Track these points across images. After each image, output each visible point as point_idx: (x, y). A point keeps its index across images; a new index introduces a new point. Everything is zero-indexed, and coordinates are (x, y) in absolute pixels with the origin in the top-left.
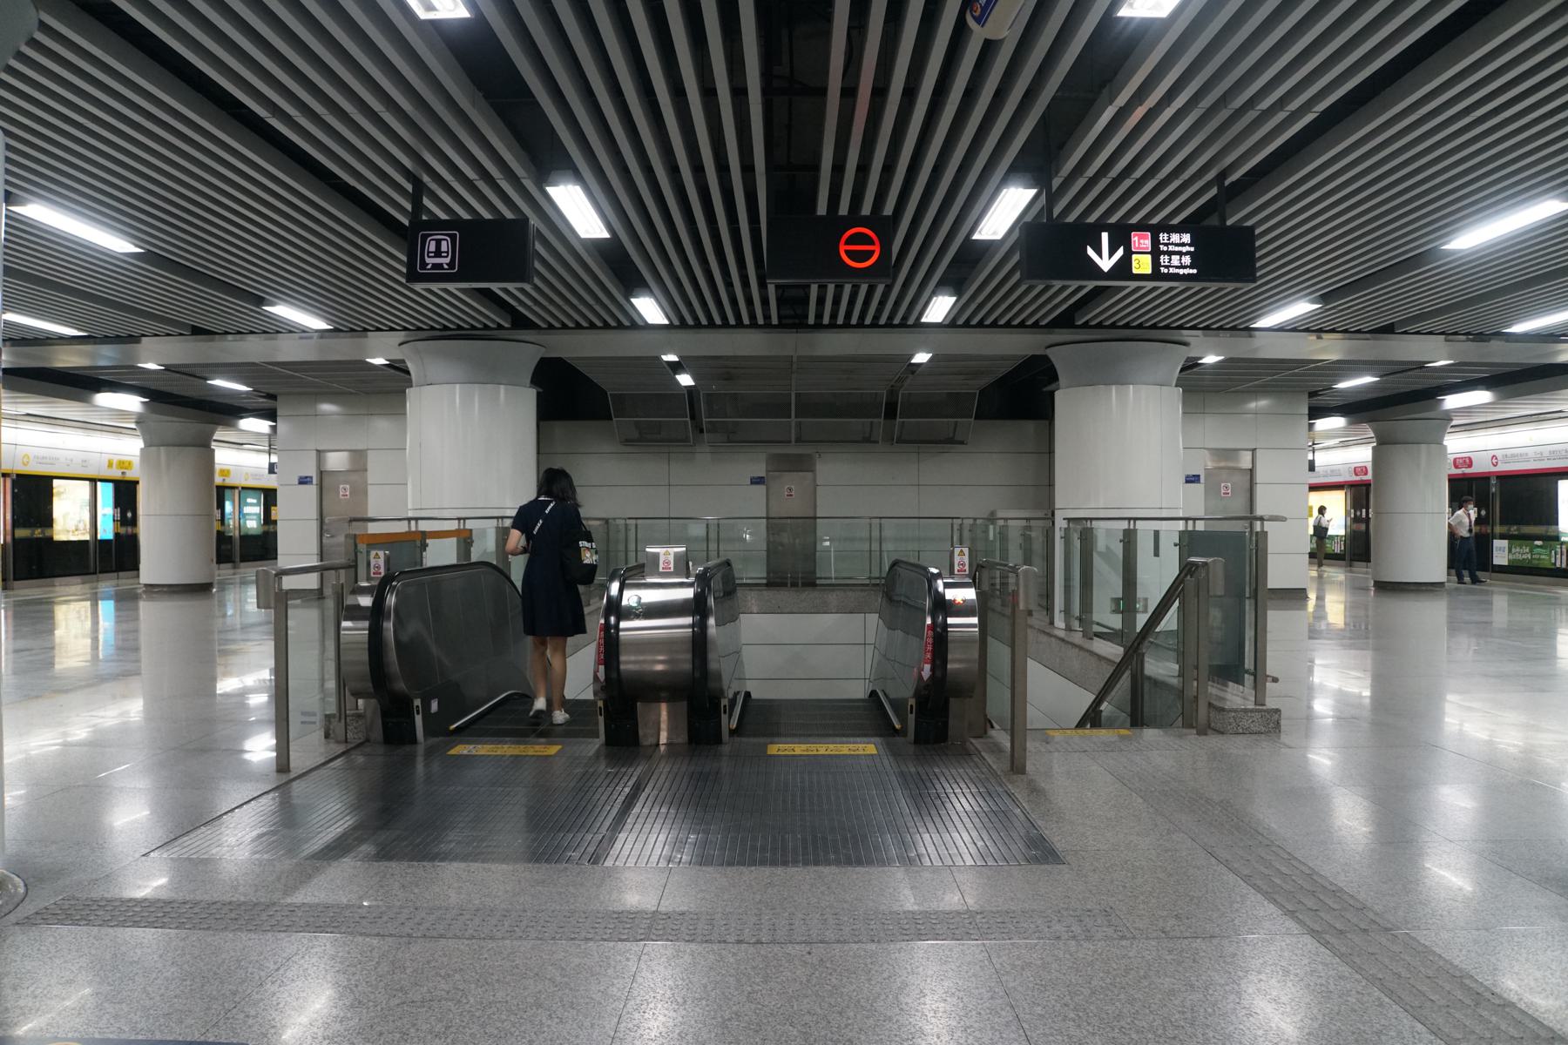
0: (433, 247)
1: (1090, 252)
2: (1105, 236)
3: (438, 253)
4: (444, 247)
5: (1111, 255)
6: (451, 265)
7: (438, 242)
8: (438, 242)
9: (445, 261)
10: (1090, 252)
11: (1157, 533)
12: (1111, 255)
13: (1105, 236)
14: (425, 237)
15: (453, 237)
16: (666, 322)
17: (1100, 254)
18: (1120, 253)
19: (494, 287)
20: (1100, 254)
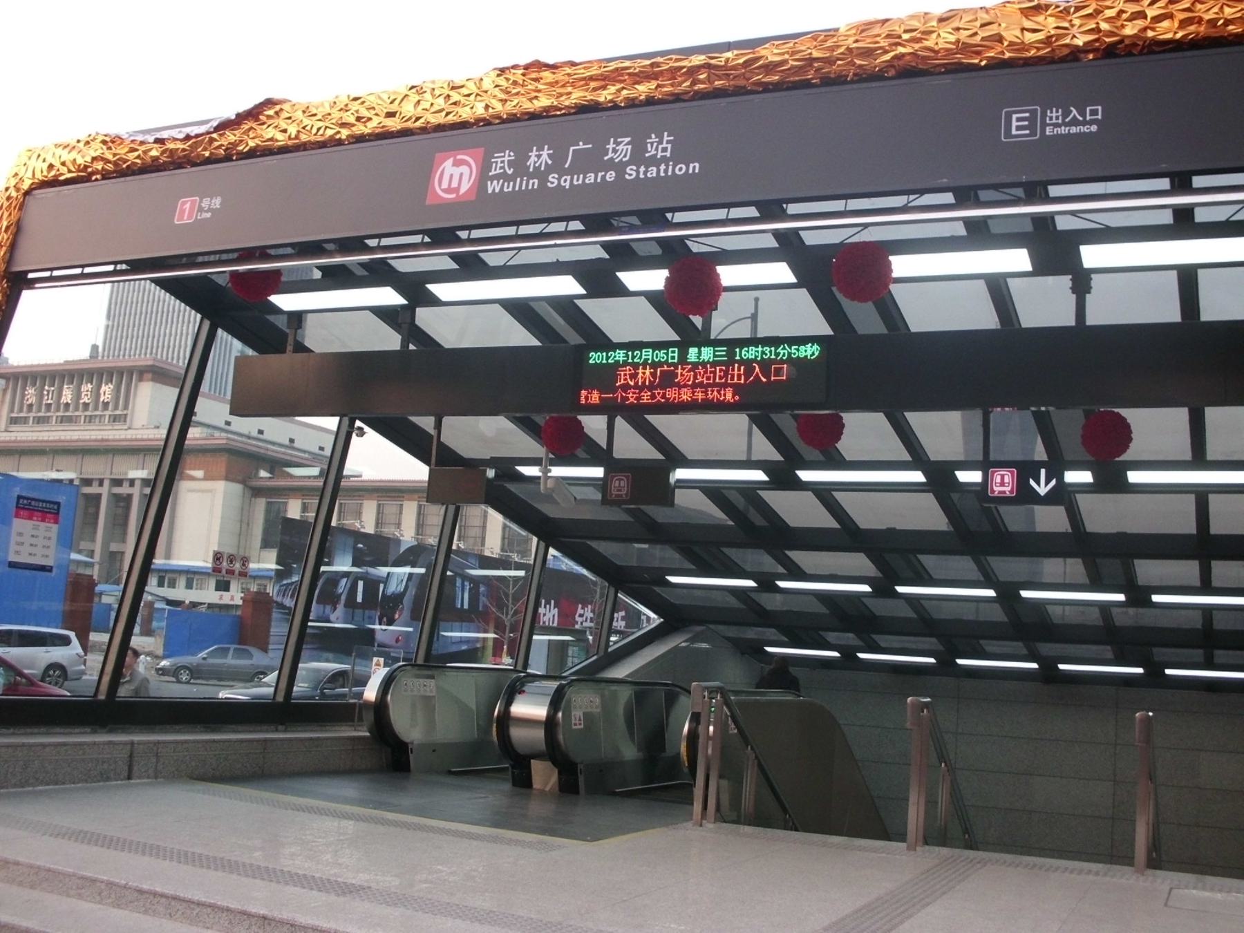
0: (998, 479)
1: (1032, 482)
2: (1043, 471)
3: (1002, 484)
4: (1007, 479)
5: (1047, 484)
6: (1011, 492)
7: (1003, 477)
8: (1003, 477)
9: (1007, 489)
10: (1032, 482)
11: (757, 300)
12: (1047, 484)
13: (1043, 471)
14: (993, 473)
15: (1012, 473)
16: (920, 557)
17: (1039, 484)
18: (1053, 482)
19: (642, 507)
20: (1039, 484)
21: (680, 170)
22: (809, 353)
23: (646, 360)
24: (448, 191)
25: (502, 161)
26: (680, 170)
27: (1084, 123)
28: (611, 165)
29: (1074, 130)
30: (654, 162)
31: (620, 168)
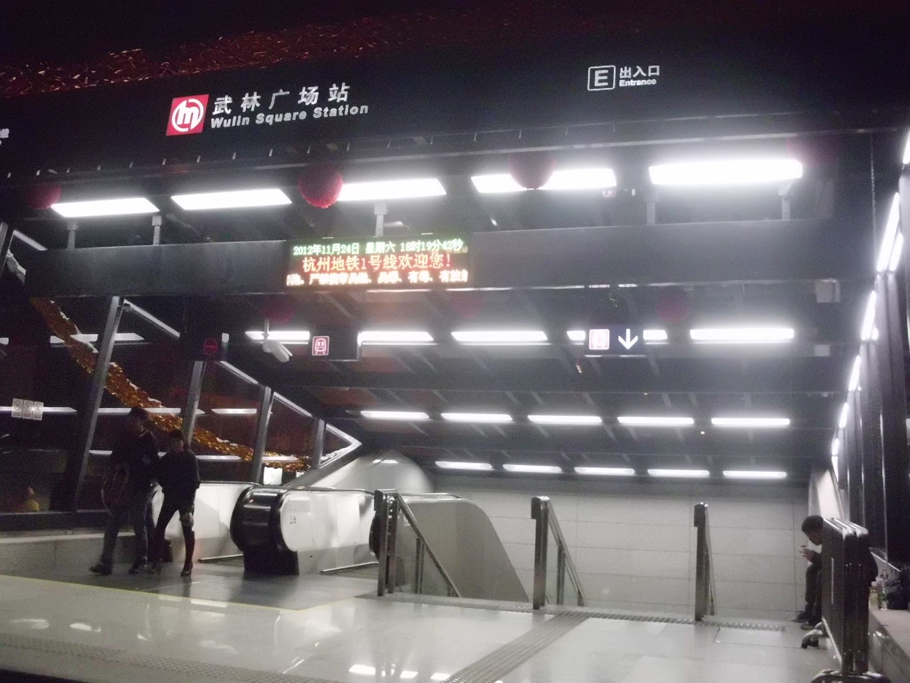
5: (632, 337)
9: (324, 350)
10: (620, 339)
12: (632, 337)
21: (354, 110)
22: (454, 247)
23: (335, 253)
24: (183, 126)
25: (223, 103)
26: (354, 110)
27: (647, 78)
28: (303, 107)
29: (639, 83)
30: (335, 104)
31: (310, 109)
